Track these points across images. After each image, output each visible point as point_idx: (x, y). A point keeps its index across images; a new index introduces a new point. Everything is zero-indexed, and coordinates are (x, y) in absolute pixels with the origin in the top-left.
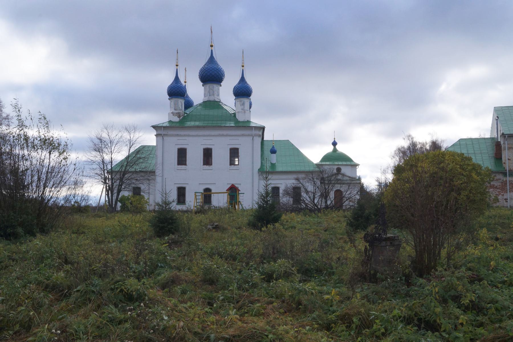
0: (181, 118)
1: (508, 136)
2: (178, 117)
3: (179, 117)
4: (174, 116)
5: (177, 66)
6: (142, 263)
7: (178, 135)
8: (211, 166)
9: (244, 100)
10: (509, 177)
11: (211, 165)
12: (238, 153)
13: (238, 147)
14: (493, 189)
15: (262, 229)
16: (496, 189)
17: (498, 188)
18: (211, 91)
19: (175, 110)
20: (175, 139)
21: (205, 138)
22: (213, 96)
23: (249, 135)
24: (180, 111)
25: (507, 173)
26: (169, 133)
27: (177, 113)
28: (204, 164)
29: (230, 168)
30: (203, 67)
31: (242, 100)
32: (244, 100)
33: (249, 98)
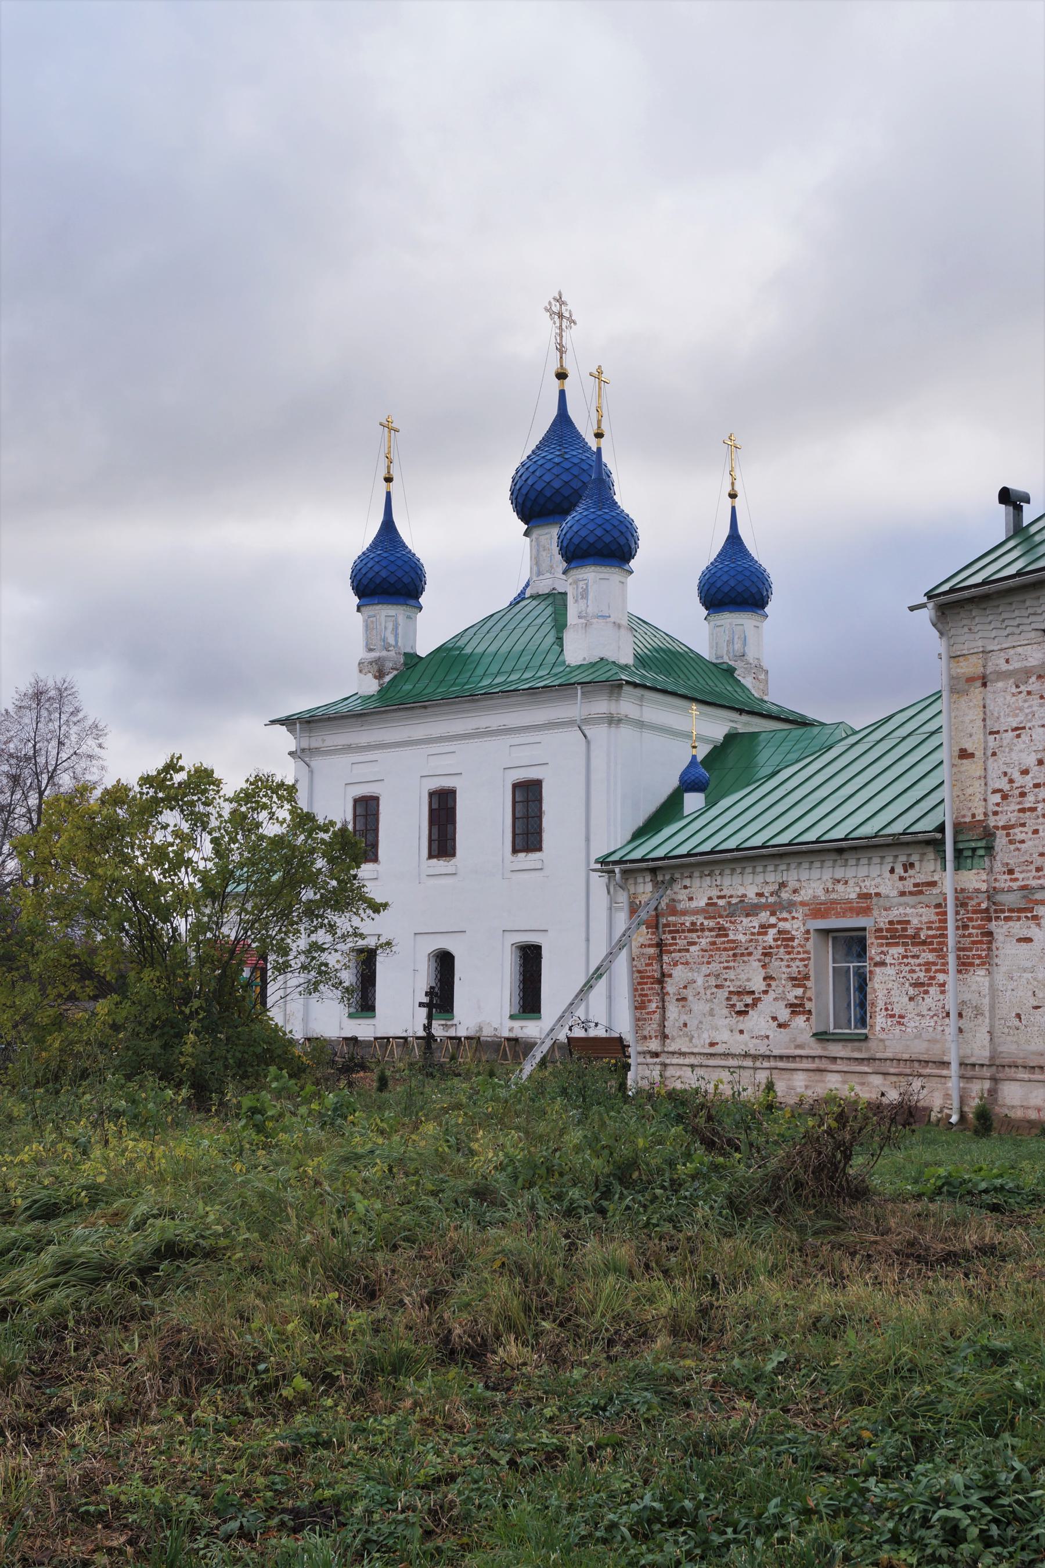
0: (387, 679)
1: (624, 872)
2: (376, 677)
3: (380, 675)
4: (362, 676)
5: (388, 480)
6: (1000, 1236)
7: (348, 749)
8: (454, 861)
9: (585, 576)
10: (957, 868)
11: (453, 854)
12: (539, 800)
13: (540, 777)
14: (901, 950)
15: (951, 1120)
16: (915, 950)
17: (924, 943)
18: (544, 554)
19: (371, 650)
20: (343, 761)
21: (435, 748)
22: (548, 575)
23: (570, 723)
24: (384, 653)
25: (942, 842)
26: (327, 744)
27: (371, 663)
28: (515, 851)
29: (432, 872)
30: (523, 465)
31: (581, 577)
32: (585, 576)
33: (626, 567)
